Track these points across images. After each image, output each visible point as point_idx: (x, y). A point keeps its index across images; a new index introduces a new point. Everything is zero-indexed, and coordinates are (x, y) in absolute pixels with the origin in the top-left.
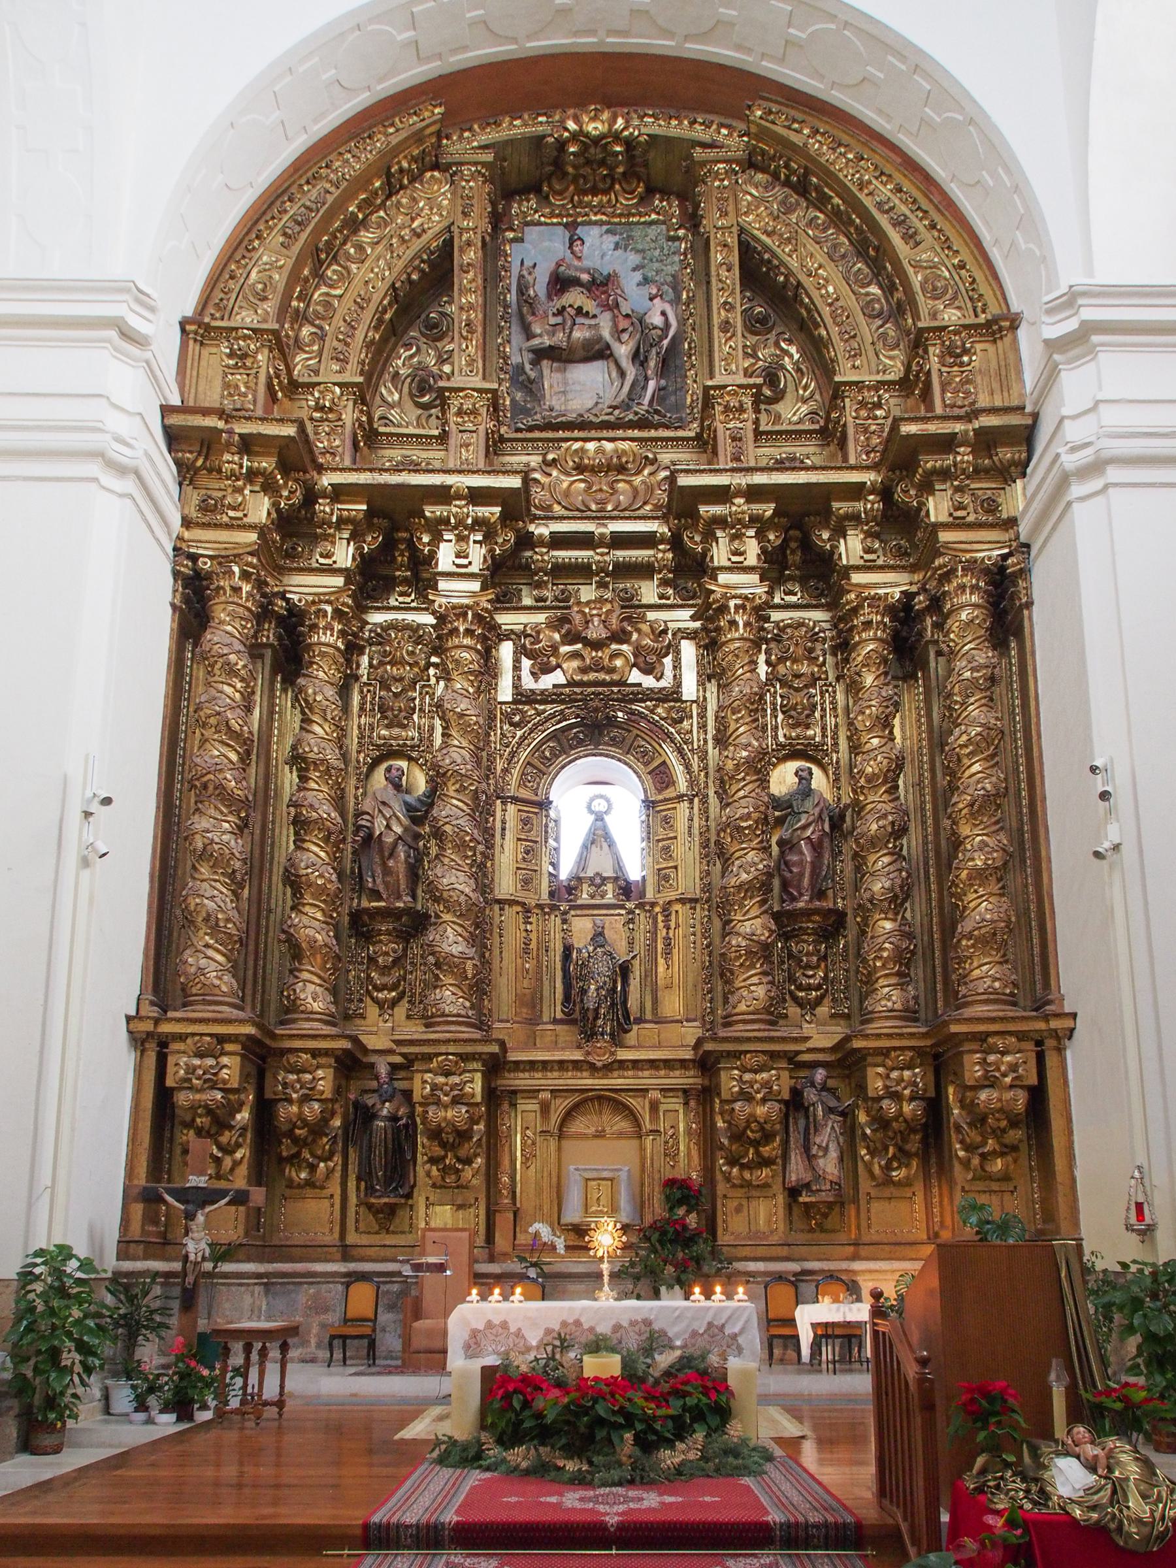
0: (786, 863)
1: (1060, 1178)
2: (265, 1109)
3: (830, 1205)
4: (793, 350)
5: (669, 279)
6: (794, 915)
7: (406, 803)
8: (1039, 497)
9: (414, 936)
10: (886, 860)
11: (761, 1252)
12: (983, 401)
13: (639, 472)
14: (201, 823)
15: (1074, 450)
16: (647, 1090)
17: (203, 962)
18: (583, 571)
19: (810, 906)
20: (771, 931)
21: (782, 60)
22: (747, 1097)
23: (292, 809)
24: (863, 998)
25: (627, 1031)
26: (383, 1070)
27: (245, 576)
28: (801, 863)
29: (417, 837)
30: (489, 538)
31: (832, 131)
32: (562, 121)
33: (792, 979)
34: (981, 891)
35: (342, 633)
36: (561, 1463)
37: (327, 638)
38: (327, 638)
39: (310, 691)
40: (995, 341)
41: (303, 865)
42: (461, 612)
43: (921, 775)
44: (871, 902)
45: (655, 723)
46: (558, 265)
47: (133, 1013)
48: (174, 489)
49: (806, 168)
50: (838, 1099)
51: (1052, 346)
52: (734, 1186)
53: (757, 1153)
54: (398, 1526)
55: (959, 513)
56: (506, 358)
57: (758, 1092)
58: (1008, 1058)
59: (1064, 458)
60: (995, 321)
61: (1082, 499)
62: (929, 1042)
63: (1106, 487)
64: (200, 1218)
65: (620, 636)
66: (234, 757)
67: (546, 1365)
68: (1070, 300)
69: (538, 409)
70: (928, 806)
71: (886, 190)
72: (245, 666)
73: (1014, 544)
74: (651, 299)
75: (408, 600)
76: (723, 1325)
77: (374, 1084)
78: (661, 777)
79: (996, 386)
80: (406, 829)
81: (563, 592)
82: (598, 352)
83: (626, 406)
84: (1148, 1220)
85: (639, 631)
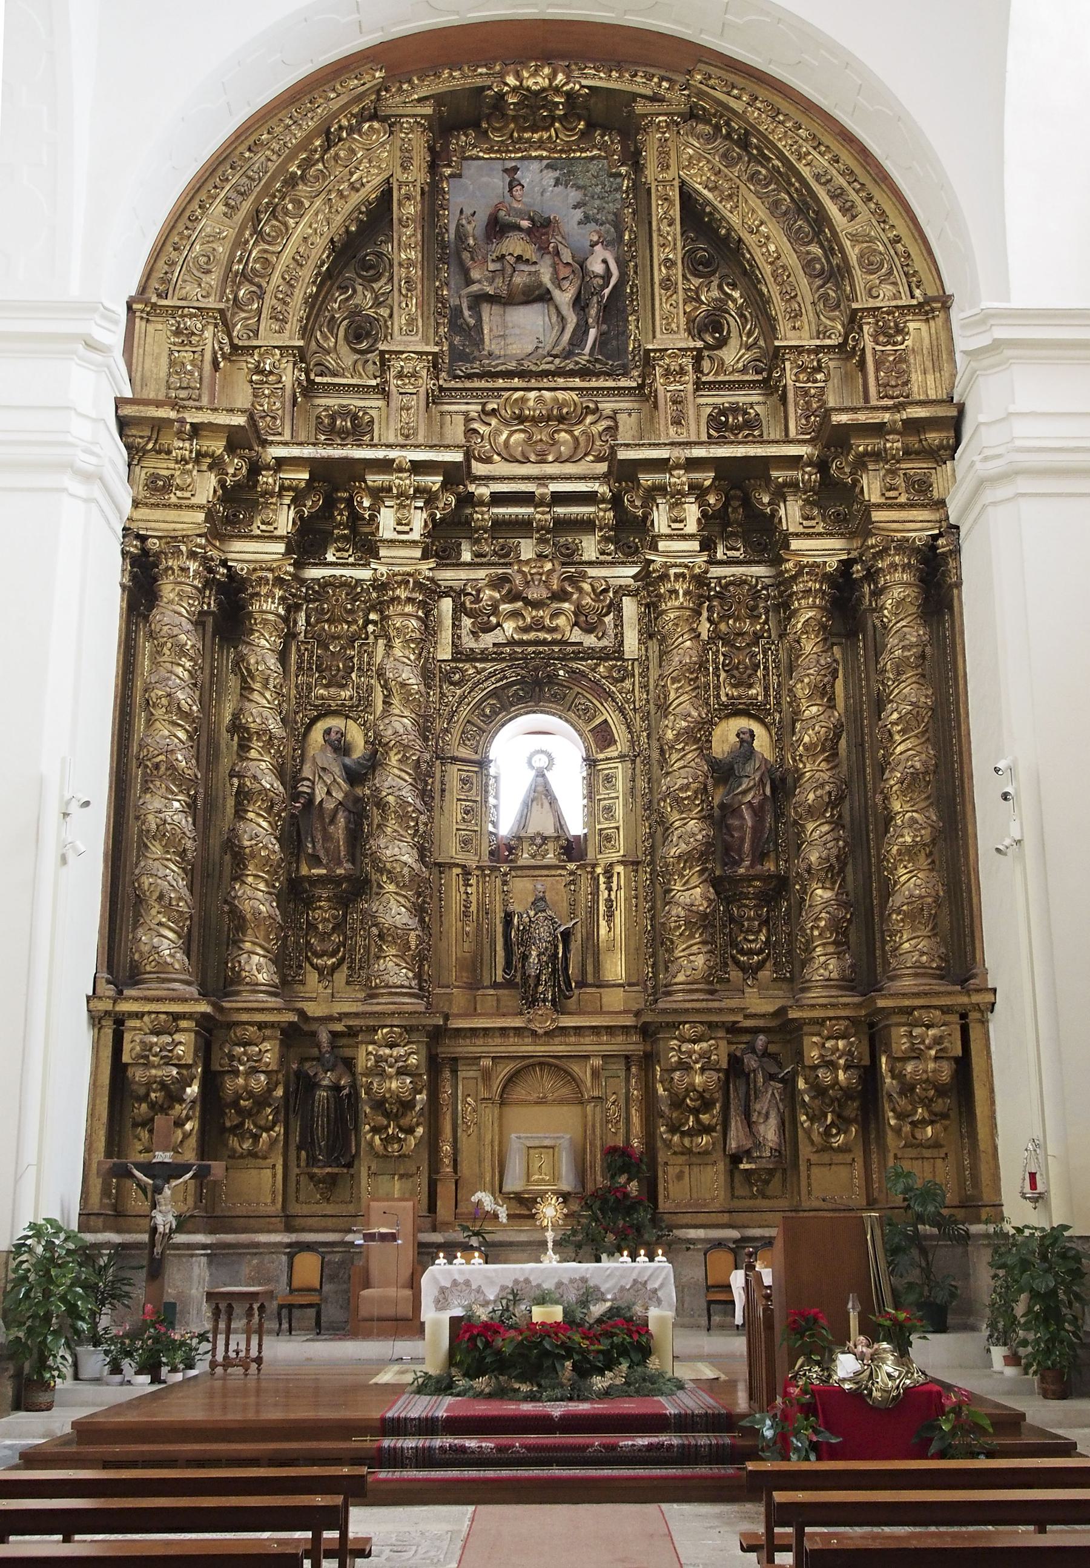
0: (728, 827)
1: (982, 1146)
2: (211, 1082)
3: (771, 1172)
4: (736, 294)
5: (611, 217)
7: (345, 767)
11: (702, 1219)
14: (154, 802)
16: (588, 1057)
19: (752, 872)
26: (324, 1037)
27: (192, 555)
28: (741, 828)
29: (358, 800)
32: (502, 75)
33: (734, 944)
36: (517, 1386)
37: (269, 606)
38: (269, 606)
39: (252, 661)
40: (927, 320)
45: (596, 683)
47: (91, 993)
49: (745, 129)
52: (675, 1153)
53: (698, 1120)
54: (406, 1419)
57: (696, 1062)
59: (978, 466)
60: (928, 301)
64: (167, 1192)
65: (561, 596)
66: (182, 735)
67: (502, 1315)
68: (986, 318)
69: (476, 353)
70: (868, 770)
72: (193, 646)
74: (592, 246)
75: (346, 555)
76: (646, 1282)
77: (315, 1052)
78: (603, 736)
79: (929, 364)
82: (538, 295)
83: (568, 354)
84: (1040, 1188)
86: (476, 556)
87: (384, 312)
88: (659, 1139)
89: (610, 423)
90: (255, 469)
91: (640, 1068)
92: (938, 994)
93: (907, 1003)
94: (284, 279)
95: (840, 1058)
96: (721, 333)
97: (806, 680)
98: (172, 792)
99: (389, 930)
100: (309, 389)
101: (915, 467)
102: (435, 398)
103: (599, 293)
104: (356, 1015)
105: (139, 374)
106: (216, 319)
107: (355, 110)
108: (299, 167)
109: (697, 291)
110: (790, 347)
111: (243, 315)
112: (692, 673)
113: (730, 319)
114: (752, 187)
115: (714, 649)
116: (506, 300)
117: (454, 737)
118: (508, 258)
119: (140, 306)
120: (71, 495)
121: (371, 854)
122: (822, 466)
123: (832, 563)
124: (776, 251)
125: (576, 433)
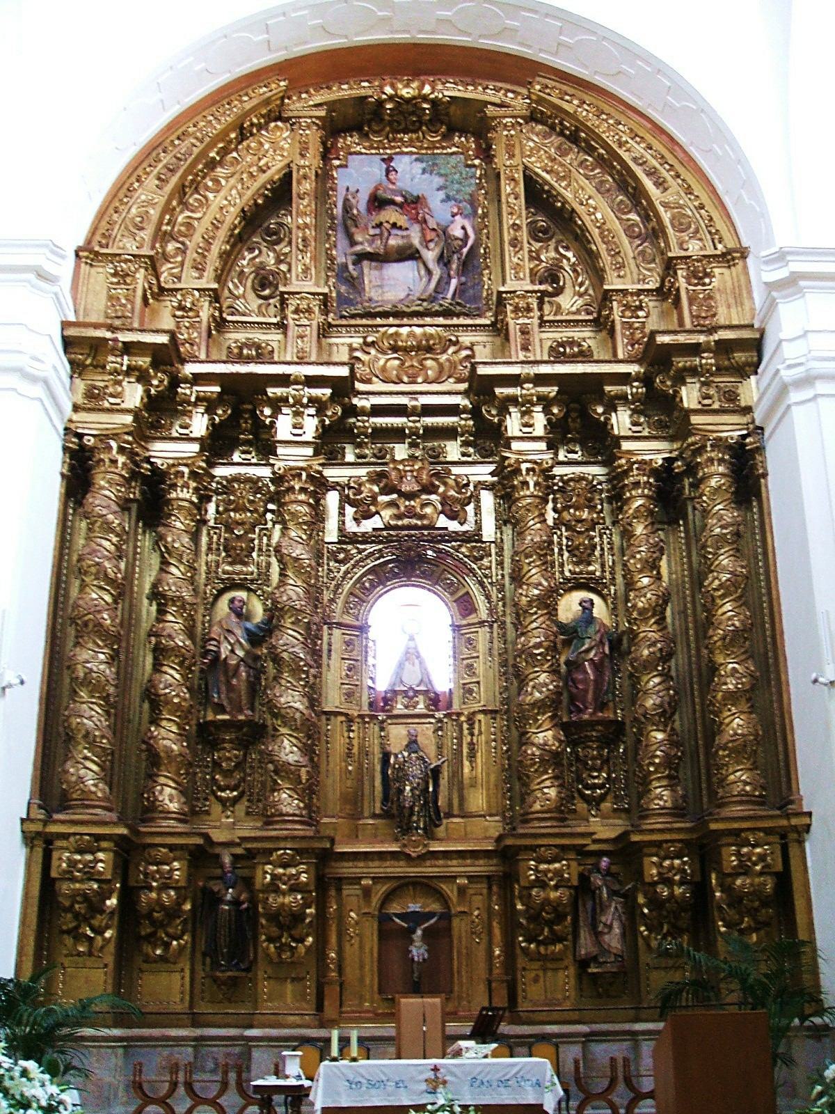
0: (573, 681)
2: (129, 896)
5: (467, 197)
6: (581, 725)
8: (770, 391)
9: (253, 743)
10: (657, 680)
12: (722, 319)
13: (444, 351)
15: (790, 367)
16: (455, 877)
17: (82, 772)
18: (397, 434)
19: (594, 718)
20: (560, 741)
21: (556, 54)
22: (542, 884)
23: (153, 639)
24: (641, 796)
25: (438, 826)
26: (227, 860)
27: (121, 450)
28: (585, 681)
29: (257, 658)
30: (320, 412)
31: (594, 101)
32: (381, 87)
33: (580, 780)
34: (734, 710)
35: (196, 490)
37: (185, 494)
38: (185, 494)
39: (169, 539)
40: (729, 267)
41: (162, 686)
42: (296, 473)
43: (685, 605)
44: (644, 716)
45: (460, 560)
46: (377, 189)
47: (25, 817)
48: (67, 381)
49: (576, 127)
50: (620, 883)
51: (770, 286)
53: (552, 931)
55: (706, 402)
56: (332, 259)
57: (551, 879)
58: (758, 850)
59: (783, 373)
61: (797, 404)
62: (695, 836)
63: (815, 397)
65: (429, 489)
66: (108, 598)
68: (781, 257)
70: (691, 632)
71: (639, 149)
73: (751, 426)
74: (453, 216)
75: (248, 456)
77: (219, 872)
78: (465, 605)
79: (732, 301)
80: (247, 653)
81: (380, 450)
82: (408, 254)
83: (432, 299)
85: (445, 484)
86: (358, 458)
87: (284, 267)
88: (518, 947)
89: (468, 352)
90: (175, 381)
91: (500, 887)
92: (761, 818)
93: (736, 825)
94: (203, 238)
95: (675, 875)
96: (558, 283)
97: (638, 556)
98: (99, 646)
99: (282, 766)
100: (220, 324)
101: (725, 380)
102: (325, 331)
103: (459, 251)
104: (255, 839)
105: (82, 307)
106: (146, 263)
107: (264, 111)
108: (218, 153)
109: (538, 252)
110: (617, 291)
111: (170, 266)
112: (542, 550)
113: (566, 274)
114: (582, 171)
115: (559, 533)
116: (380, 259)
117: (339, 606)
118: (385, 224)
119: (86, 254)
120: (30, 330)
121: (268, 702)
122: (647, 380)
123: (659, 460)
124: (603, 218)
125: (441, 361)
